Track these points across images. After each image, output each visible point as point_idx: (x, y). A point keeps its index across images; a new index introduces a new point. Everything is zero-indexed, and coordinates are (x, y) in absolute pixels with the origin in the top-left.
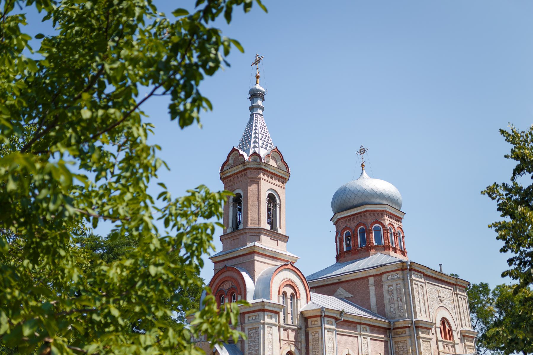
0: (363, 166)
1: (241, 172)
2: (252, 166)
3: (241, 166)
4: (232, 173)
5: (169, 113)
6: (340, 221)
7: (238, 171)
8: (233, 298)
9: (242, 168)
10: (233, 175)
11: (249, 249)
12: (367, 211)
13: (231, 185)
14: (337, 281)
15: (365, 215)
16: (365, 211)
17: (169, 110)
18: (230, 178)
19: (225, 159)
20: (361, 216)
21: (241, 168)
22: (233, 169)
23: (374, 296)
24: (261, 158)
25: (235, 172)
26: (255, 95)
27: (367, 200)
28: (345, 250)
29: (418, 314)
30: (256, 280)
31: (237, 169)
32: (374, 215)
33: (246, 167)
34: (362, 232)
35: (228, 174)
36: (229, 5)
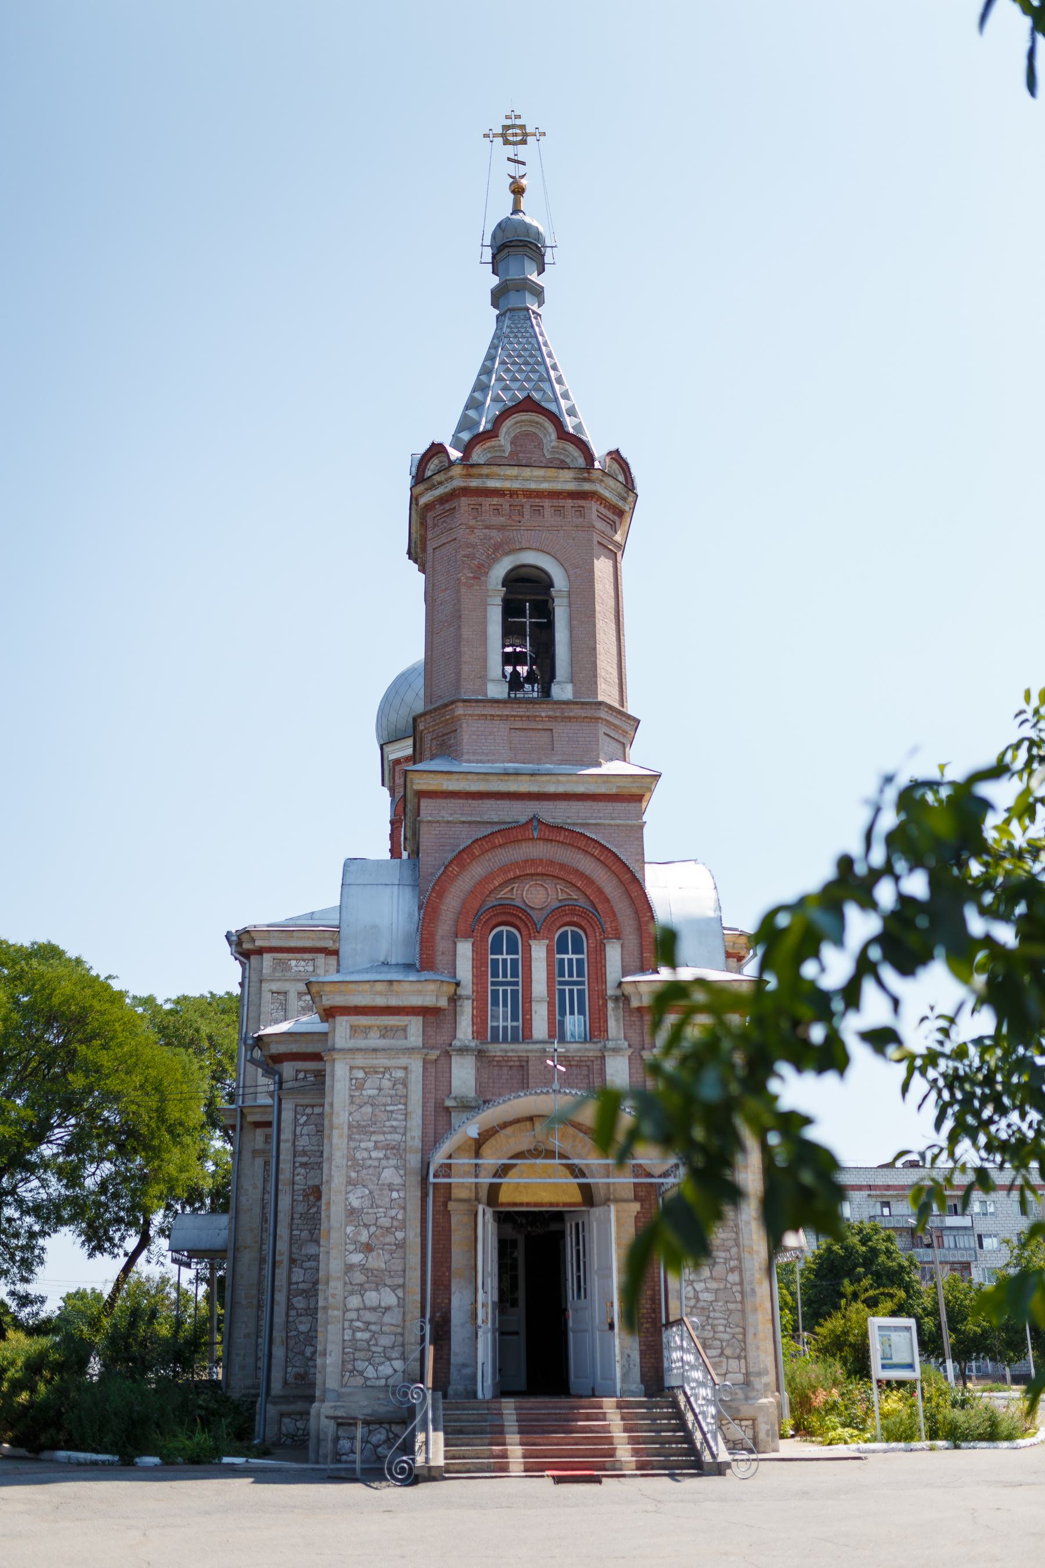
2: (607, 494)
4: (516, 485)
5: (22, 946)
7: (545, 486)
8: (877, 1257)
9: (572, 486)
10: (513, 493)
11: (623, 783)
13: (502, 528)
17: (61, 948)
18: (495, 501)
21: (566, 481)
22: (527, 472)
23: (600, 636)
24: (589, 458)
25: (533, 486)
26: (516, 248)
31: (545, 479)
33: (587, 487)
35: (492, 484)
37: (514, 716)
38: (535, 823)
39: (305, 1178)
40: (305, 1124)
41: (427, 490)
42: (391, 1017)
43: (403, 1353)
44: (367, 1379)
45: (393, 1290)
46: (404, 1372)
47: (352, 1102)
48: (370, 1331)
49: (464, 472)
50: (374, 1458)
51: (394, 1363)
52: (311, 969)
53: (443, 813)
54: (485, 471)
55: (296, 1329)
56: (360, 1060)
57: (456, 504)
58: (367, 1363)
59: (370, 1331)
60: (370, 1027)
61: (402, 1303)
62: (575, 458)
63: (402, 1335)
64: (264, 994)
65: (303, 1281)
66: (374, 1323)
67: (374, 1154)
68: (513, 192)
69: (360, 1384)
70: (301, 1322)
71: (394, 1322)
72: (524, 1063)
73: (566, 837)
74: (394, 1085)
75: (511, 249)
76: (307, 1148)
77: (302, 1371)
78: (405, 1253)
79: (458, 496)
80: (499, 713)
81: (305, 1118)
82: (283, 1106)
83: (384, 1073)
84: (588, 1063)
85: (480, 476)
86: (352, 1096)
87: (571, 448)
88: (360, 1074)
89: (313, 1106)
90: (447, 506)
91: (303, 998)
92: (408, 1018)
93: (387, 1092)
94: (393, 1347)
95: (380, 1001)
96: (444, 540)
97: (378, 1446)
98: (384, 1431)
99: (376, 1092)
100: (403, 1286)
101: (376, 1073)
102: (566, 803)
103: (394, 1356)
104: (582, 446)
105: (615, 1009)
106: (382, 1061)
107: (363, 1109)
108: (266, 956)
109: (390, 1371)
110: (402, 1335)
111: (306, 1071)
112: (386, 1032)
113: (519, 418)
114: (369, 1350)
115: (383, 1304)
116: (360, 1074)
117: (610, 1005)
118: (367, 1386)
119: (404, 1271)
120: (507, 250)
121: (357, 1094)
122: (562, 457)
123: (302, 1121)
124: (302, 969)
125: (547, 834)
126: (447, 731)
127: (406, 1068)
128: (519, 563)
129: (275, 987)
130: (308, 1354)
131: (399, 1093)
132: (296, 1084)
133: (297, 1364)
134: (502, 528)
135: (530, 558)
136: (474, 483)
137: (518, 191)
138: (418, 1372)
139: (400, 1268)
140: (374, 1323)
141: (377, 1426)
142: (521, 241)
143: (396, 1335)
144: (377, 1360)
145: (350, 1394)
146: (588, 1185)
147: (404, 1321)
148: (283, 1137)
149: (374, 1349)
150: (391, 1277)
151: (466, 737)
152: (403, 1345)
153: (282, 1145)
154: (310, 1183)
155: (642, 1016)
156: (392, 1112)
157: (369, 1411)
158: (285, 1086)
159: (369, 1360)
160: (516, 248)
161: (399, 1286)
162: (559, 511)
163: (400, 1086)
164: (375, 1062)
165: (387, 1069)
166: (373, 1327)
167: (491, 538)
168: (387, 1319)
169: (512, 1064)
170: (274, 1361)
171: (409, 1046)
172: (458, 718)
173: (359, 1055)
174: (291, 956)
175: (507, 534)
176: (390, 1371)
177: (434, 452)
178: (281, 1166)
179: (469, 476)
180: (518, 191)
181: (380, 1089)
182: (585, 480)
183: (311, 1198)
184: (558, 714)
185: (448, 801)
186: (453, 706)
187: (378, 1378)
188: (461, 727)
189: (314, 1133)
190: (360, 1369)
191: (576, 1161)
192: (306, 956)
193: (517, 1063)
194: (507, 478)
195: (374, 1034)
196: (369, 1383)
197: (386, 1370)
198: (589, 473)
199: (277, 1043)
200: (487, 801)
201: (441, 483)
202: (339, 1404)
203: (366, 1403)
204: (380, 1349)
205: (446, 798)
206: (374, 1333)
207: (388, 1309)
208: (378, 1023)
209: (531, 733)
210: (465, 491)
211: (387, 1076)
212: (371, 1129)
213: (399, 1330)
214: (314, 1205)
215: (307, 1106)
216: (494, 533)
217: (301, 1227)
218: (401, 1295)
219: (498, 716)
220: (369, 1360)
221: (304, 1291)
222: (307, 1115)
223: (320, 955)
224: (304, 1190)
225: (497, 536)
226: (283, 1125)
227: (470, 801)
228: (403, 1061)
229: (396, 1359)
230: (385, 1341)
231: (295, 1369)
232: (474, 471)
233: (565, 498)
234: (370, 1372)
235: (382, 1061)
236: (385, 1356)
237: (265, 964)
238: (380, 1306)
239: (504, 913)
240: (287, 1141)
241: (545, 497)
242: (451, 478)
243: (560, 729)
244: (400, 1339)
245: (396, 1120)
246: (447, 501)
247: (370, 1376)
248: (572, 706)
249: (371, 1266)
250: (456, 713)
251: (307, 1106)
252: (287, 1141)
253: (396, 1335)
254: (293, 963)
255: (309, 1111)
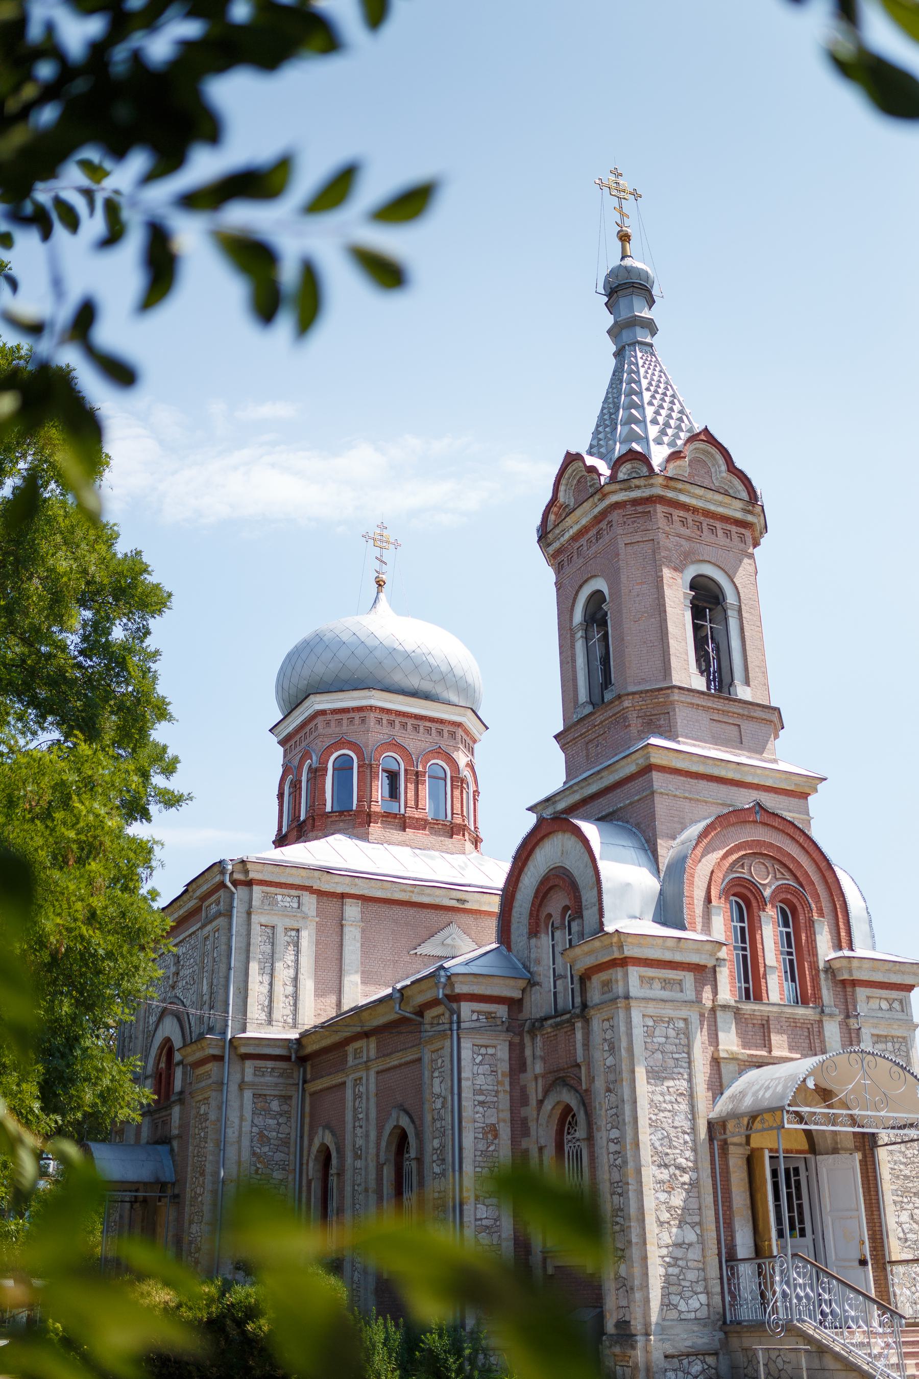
0: (380, 584)
3: (739, 505)
4: (699, 504)
7: (721, 510)
9: (739, 515)
10: (695, 510)
12: (371, 708)
14: (454, 903)
15: (363, 720)
16: (360, 709)
20: (339, 721)
25: (712, 508)
27: (439, 690)
28: (328, 808)
29: (255, 1012)
31: (721, 504)
32: (440, 733)
34: (343, 768)
35: (683, 498)
36: (847, 50)
38: (757, 808)
39: (484, 1116)
40: (481, 1064)
41: (621, 489)
42: (670, 971)
43: (706, 1287)
44: (680, 1312)
45: (693, 1227)
48: (679, 1266)
49: (665, 483)
51: (700, 1296)
52: (296, 905)
54: (680, 485)
56: (651, 1009)
57: (651, 509)
58: (679, 1297)
59: (679, 1266)
60: (653, 979)
61: (701, 1239)
62: (739, 491)
63: (703, 1270)
65: (486, 1218)
67: (668, 1098)
69: (676, 1317)
73: (779, 823)
74: (678, 1034)
75: (635, 290)
76: (483, 1087)
78: (699, 1192)
79: (655, 502)
80: (704, 704)
81: (480, 1058)
82: (462, 1045)
83: (668, 1022)
85: (674, 489)
86: (645, 1042)
87: (737, 482)
88: (651, 1023)
89: (486, 1047)
90: (640, 509)
91: (289, 933)
92: (683, 973)
93: (671, 1040)
94: (697, 1282)
95: (668, 956)
98: (699, 1362)
99: (663, 1040)
100: (700, 1224)
101: (663, 1021)
102: (736, 788)
103: (699, 1290)
104: (746, 482)
105: (826, 979)
108: (255, 888)
109: (698, 1305)
110: (703, 1270)
111: (479, 1013)
112: (666, 983)
113: (697, 446)
115: (686, 1241)
116: (651, 1023)
117: (822, 976)
119: (700, 1209)
122: (726, 488)
123: (478, 1061)
124: (288, 905)
126: (656, 712)
127: (685, 1020)
128: (700, 572)
129: (263, 920)
131: (682, 1043)
132: (473, 1025)
134: (689, 539)
135: (708, 570)
136: (670, 494)
137: (624, 238)
138: (721, 1305)
139: (696, 1207)
141: (694, 1358)
142: (641, 284)
143: (698, 1270)
144: (688, 1294)
145: (671, 1327)
147: (704, 1257)
148: (463, 1075)
149: (683, 1283)
150: (690, 1215)
151: (679, 721)
152: (705, 1280)
153: (464, 1083)
154: (488, 1121)
155: (845, 987)
156: (677, 1059)
158: (463, 1025)
159: (680, 1294)
161: (697, 1224)
163: (682, 1036)
165: (671, 1020)
166: (680, 1263)
168: (691, 1255)
169: (755, 1022)
171: (686, 999)
172: (672, 703)
173: (651, 1004)
174: (278, 890)
176: (698, 1305)
178: (463, 1103)
179: (667, 487)
180: (624, 238)
181: (667, 1038)
182: (749, 512)
183: (490, 1136)
184: (746, 713)
186: (669, 691)
190: (675, 1303)
191: (856, 1112)
192: (294, 892)
193: (760, 1022)
194: (694, 496)
195: (657, 985)
196: (683, 1317)
197: (694, 1303)
198: (753, 507)
199: (462, 983)
201: (638, 487)
202: (664, 1337)
203: (686, 1336)
204: (688, 1284)
207: (690, 1245)
208: (660, 975)
209: (723, 726)
210: (661, 500)
211: (671, 1026)
213: (701, 1266)
214: (492, 1143)
215: (482, 1046)
216: (683, 542)
217: (482, 1164)
218: (698, 1232)
219: (702, 706)
220: (680, 1294)
221: (487, 1227)
223: (305, 893)
224: (483, 1128)
225: (686, 545)
226: (463, 1063)
227: (689, 780)
228: (684, 1013)
229: (701, 1293)
230: (692, 1275)
232: (672, 483)
233: (731, 524)
234: (683, 1306)
236: (692, 1291)
237: (255, 895)
238: (684, 1243)
239: (745, 887)
240: (468, 1079)
242: (652, 485)
243: (746, 726)
244: (702, 1274)
245: (681, 1067)
246: (640, 504)
247: (683, 1310)
248: (756, 708)
249: (674, 1205)
250: (671, 698)
251: (482, 1046)
252: (468, 1079)
255: (483, 1051)
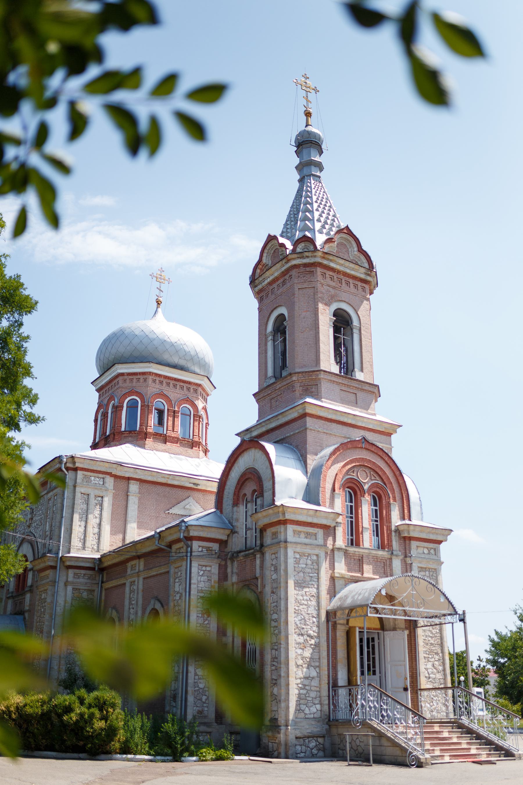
1: (355, 278)
3: (363, 270)
6: (121, 378)
7: (353, 273)
9: (363, 276)
10: (339, 272)
12: (150, 373)
15: (145, 380)
16: (144, 374)
19: (364, 248)
20: (132, 380)
25: (348, 271)
26: (307, 144)
28: (123, 429)
30: (309, 471)
31: (353, 269)
34: (132, 406)
35: (332, 265)
37: (342, 384)
38: (363, 440)
40: (202, 575)
41: (298, 258)
42: (310, 528)
43: (320, 701)
44: (306, 714)
45: (315, 669)
46: (321, 711)
47: (295, 570)
48: (306, 689)
49: (322, 255)
50: (311, 755)
52: (101, 483)
53: (316, 426)
54: (331, 257)
55: (198, 686)
59: (306, 689)
60: (300, 532)
61: (319, 675)
62: (363, 263)
63: (319, 692)
64: (77, 494)
66: (308, 685)
67: (305, 598)
68: (306, 115)
70: (200, 683)
71: (316, 685)
72: (360, 558)
73: (375, 449)
75: (312, 145)
76: (203, 589)
77: (200, 709)
79: (316, 266)
80: (337, 381)
81: (202, 572)
82: (193, 565)
83: (308, 556)
84: (385, 561)
86: (294, 567)
87: (363, 258)
88: (298, 556)
89: (206, 566)
91: (97, 499)
95: (309, 520)
96: (305, 285)
97: (312, 749)
98: (314, 741)
100: (319, 667)
101: (305, 556)
105: (395, 536)
106: (308, 550)
107: (300, 574)
110: (319, 692)
111: (203, 547)
112: (308, 535)
114: (306, 699)
115: (311, 676)
117: (393, 534)
118: (306, 718)
119: (319, 659)
120: (310, 144)
121: (296, 566)
122: (357, 260)
123: (201, 574)
124: (97, 482)
125: (368, 446)
126: (310, 384)
127: (317, 555)
128: (339, 307)
129: (83, 490)
130: (204, 700)
131: (315, 568)
132: (199, 554)
133: (198, 705)
134: (334, 288)
135: (344, 306)
136: (325, 262)
138: (328, 710)
139: (317, 657)
140: (308, 685)
141: (312, 739)
143: (317, 691)
144: (310, 704)
146: (382, 618)
147: (320, 685)
149: (308, 698)
150: (314, 662)
151: (323, 389)
152: (320, 697)
153: (192, 586)
156: (311, 577)
157: (309, 731)
158: (193, 554)
160: (307, 144)
161: (317, 666)
162: (356, 286)
163: (315, 564)
164: (305, 550)
165: (309, 555)
166: (307, 687)
167: (330, 291)
169: (355, 558)
170: (188, 704)
171: (318, 544)
172: (319, 379)
173: (299, 546)
174: (92, 474)
175: (336, 291)
176: (315, 710)
177: (304, 240)
179: (323, 258)
180: (308, 114)
181: (306, 565)
183: (205, 616)
184: (360, 387)
185: (317, 420)
186: (318, 373)
187: (310, 714)
188: (321, 383)
189: (206, 581)
191: (407, 608)
192: (101, 476)
193: (358, 558)
195: (303, 535)
196: (307, 717)
197: (313, 710)
198: (371, 272)
199: (194, 530)
200: (333, 424)
201: (308, 257)
205: (317, 418)
206: (308, 690)
207: (313, 678)
208: (305, 530)
210: (320, 265)
211: (309, 558)
212: (303, 585)
213: (318, 689)
214: (207, 620)
215: (203, 566)
216: (331, 289)
218: (318, 671)
219: (336, 382)
222: (203, 571)
225: (332, 291)
226: (192, 575)
228: (316, 551)
229: (317, 704)
230: (313, 694)
231: (197, 708)
232: (327, 256)
233: (358, 281)
234: (307, 711)
235: (308, 550)
237: (78, 476)
238: (310, 677)
239: (354, 483)
240: (195, 584)
241: (351, 278)
242: (315, 256)
244: (318, 694)
245: (314, 581)
246: (308, 267)
247: (307, 713)
251: (203, 566)
252: (195, 584)
253: (317, 691)
254: (93, 478)
255: (204, 568)
